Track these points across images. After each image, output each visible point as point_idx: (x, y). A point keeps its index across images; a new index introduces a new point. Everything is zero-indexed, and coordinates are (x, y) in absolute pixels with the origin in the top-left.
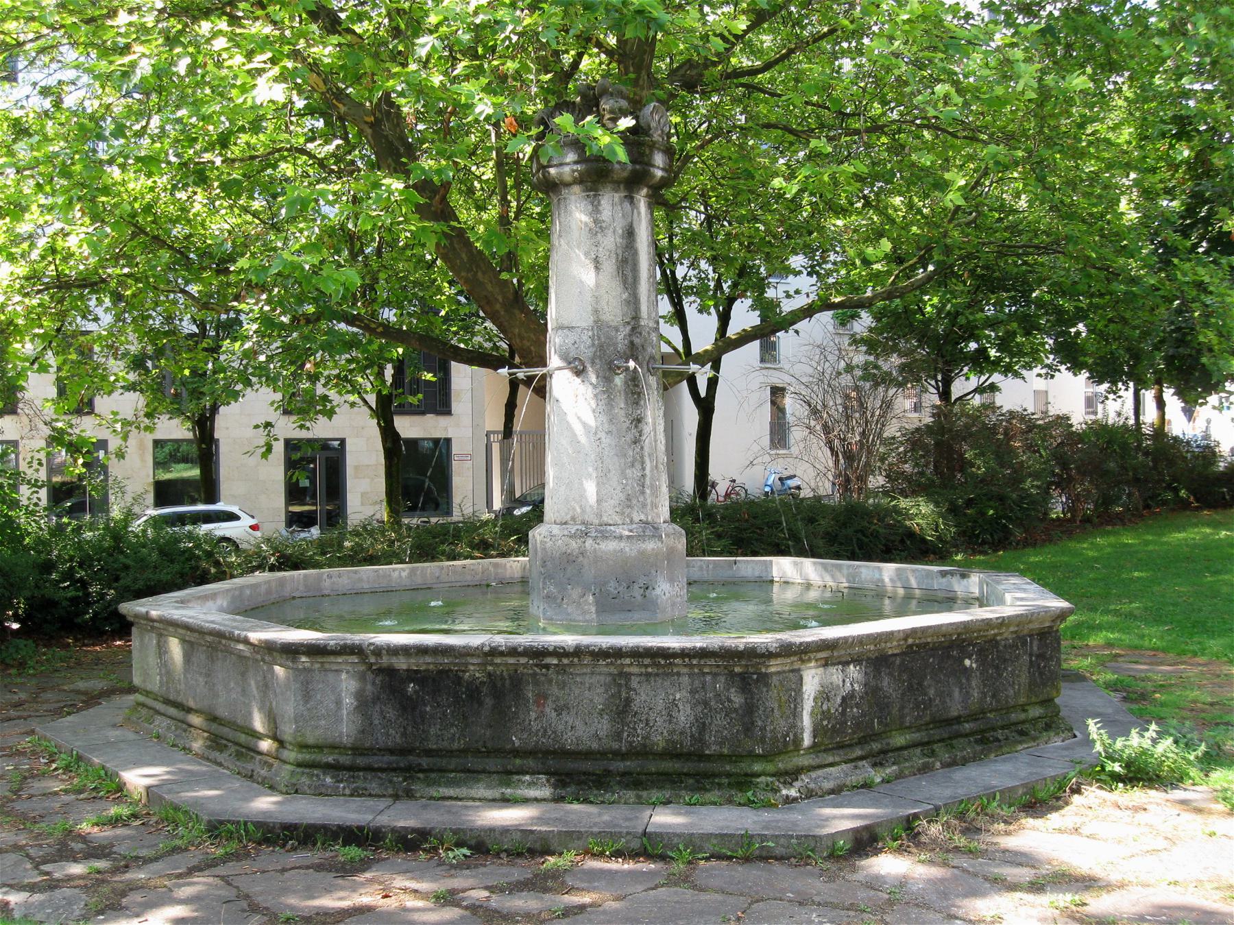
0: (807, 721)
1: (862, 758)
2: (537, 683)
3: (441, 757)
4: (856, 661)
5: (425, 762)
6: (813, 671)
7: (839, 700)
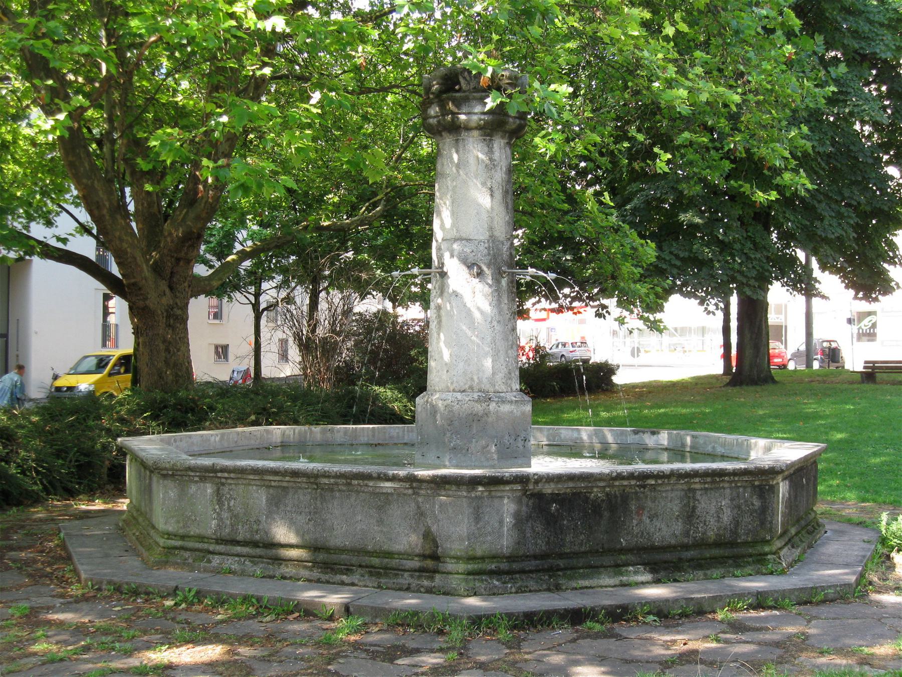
2: (638, 499)
3: (570, 558)
5: (561, 563)
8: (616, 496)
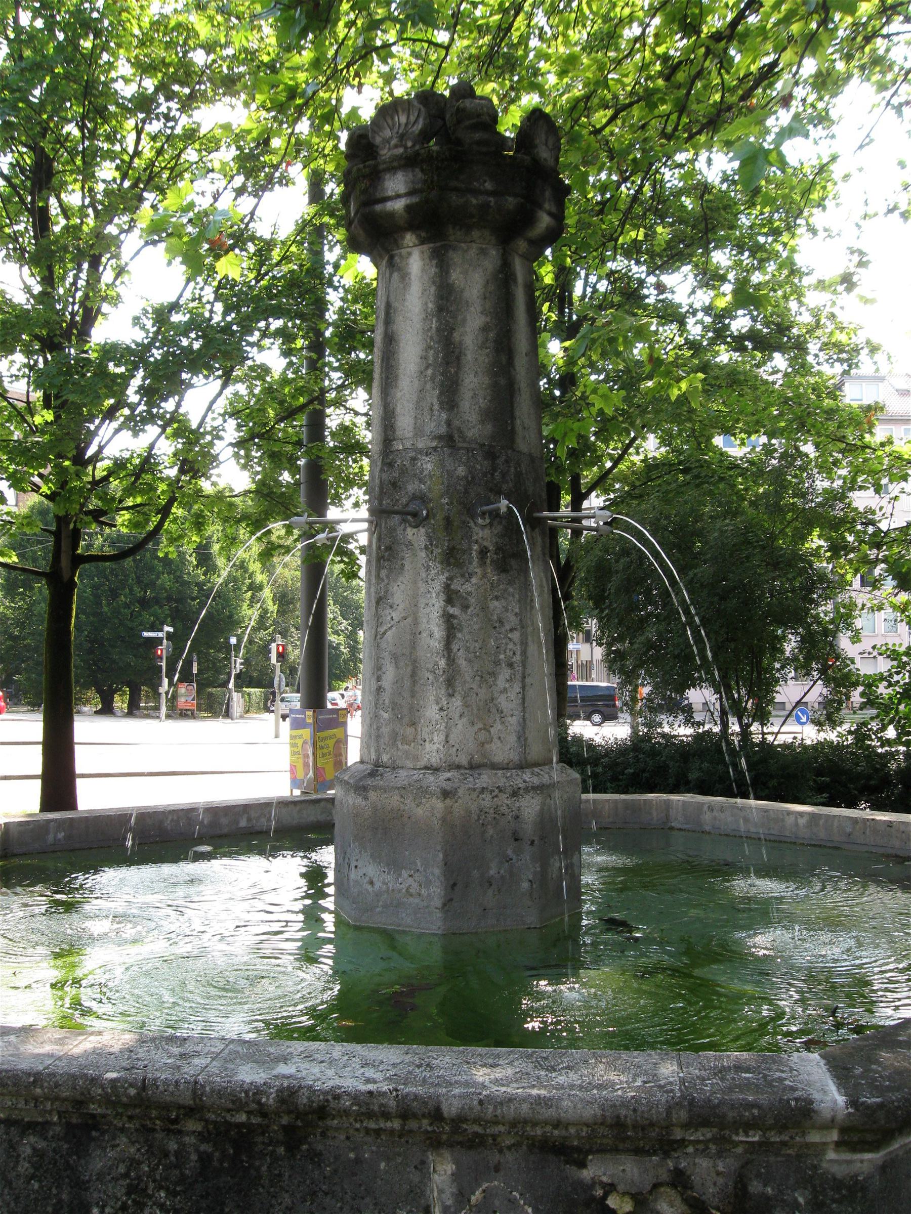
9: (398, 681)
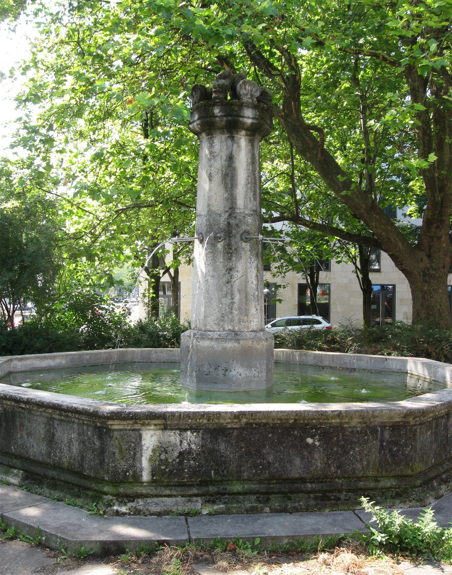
0: (145, 463)
1: (197, 495)
4: (193, 429)
6: (152, 432)
7: (176, 454)
8: (9, 413)
9: (241, 299)
